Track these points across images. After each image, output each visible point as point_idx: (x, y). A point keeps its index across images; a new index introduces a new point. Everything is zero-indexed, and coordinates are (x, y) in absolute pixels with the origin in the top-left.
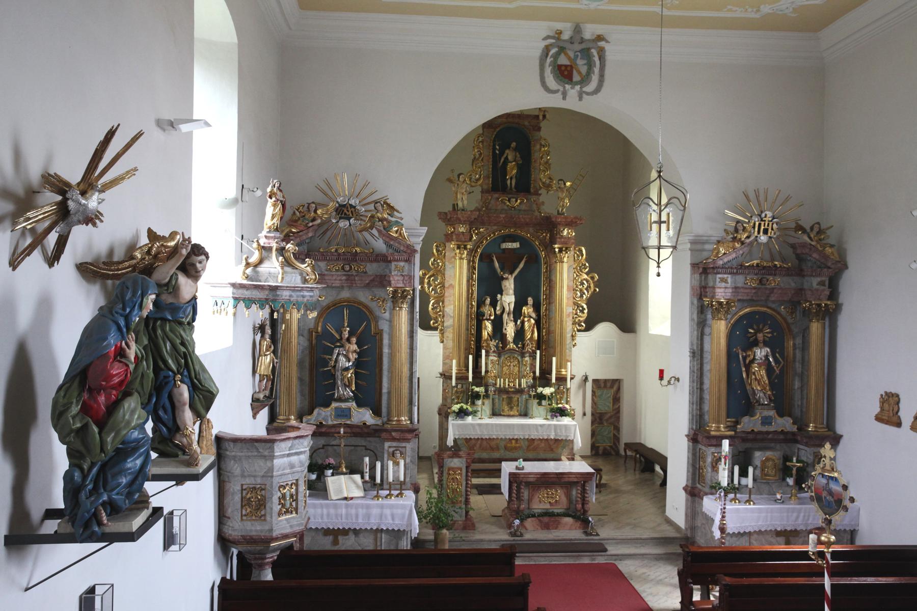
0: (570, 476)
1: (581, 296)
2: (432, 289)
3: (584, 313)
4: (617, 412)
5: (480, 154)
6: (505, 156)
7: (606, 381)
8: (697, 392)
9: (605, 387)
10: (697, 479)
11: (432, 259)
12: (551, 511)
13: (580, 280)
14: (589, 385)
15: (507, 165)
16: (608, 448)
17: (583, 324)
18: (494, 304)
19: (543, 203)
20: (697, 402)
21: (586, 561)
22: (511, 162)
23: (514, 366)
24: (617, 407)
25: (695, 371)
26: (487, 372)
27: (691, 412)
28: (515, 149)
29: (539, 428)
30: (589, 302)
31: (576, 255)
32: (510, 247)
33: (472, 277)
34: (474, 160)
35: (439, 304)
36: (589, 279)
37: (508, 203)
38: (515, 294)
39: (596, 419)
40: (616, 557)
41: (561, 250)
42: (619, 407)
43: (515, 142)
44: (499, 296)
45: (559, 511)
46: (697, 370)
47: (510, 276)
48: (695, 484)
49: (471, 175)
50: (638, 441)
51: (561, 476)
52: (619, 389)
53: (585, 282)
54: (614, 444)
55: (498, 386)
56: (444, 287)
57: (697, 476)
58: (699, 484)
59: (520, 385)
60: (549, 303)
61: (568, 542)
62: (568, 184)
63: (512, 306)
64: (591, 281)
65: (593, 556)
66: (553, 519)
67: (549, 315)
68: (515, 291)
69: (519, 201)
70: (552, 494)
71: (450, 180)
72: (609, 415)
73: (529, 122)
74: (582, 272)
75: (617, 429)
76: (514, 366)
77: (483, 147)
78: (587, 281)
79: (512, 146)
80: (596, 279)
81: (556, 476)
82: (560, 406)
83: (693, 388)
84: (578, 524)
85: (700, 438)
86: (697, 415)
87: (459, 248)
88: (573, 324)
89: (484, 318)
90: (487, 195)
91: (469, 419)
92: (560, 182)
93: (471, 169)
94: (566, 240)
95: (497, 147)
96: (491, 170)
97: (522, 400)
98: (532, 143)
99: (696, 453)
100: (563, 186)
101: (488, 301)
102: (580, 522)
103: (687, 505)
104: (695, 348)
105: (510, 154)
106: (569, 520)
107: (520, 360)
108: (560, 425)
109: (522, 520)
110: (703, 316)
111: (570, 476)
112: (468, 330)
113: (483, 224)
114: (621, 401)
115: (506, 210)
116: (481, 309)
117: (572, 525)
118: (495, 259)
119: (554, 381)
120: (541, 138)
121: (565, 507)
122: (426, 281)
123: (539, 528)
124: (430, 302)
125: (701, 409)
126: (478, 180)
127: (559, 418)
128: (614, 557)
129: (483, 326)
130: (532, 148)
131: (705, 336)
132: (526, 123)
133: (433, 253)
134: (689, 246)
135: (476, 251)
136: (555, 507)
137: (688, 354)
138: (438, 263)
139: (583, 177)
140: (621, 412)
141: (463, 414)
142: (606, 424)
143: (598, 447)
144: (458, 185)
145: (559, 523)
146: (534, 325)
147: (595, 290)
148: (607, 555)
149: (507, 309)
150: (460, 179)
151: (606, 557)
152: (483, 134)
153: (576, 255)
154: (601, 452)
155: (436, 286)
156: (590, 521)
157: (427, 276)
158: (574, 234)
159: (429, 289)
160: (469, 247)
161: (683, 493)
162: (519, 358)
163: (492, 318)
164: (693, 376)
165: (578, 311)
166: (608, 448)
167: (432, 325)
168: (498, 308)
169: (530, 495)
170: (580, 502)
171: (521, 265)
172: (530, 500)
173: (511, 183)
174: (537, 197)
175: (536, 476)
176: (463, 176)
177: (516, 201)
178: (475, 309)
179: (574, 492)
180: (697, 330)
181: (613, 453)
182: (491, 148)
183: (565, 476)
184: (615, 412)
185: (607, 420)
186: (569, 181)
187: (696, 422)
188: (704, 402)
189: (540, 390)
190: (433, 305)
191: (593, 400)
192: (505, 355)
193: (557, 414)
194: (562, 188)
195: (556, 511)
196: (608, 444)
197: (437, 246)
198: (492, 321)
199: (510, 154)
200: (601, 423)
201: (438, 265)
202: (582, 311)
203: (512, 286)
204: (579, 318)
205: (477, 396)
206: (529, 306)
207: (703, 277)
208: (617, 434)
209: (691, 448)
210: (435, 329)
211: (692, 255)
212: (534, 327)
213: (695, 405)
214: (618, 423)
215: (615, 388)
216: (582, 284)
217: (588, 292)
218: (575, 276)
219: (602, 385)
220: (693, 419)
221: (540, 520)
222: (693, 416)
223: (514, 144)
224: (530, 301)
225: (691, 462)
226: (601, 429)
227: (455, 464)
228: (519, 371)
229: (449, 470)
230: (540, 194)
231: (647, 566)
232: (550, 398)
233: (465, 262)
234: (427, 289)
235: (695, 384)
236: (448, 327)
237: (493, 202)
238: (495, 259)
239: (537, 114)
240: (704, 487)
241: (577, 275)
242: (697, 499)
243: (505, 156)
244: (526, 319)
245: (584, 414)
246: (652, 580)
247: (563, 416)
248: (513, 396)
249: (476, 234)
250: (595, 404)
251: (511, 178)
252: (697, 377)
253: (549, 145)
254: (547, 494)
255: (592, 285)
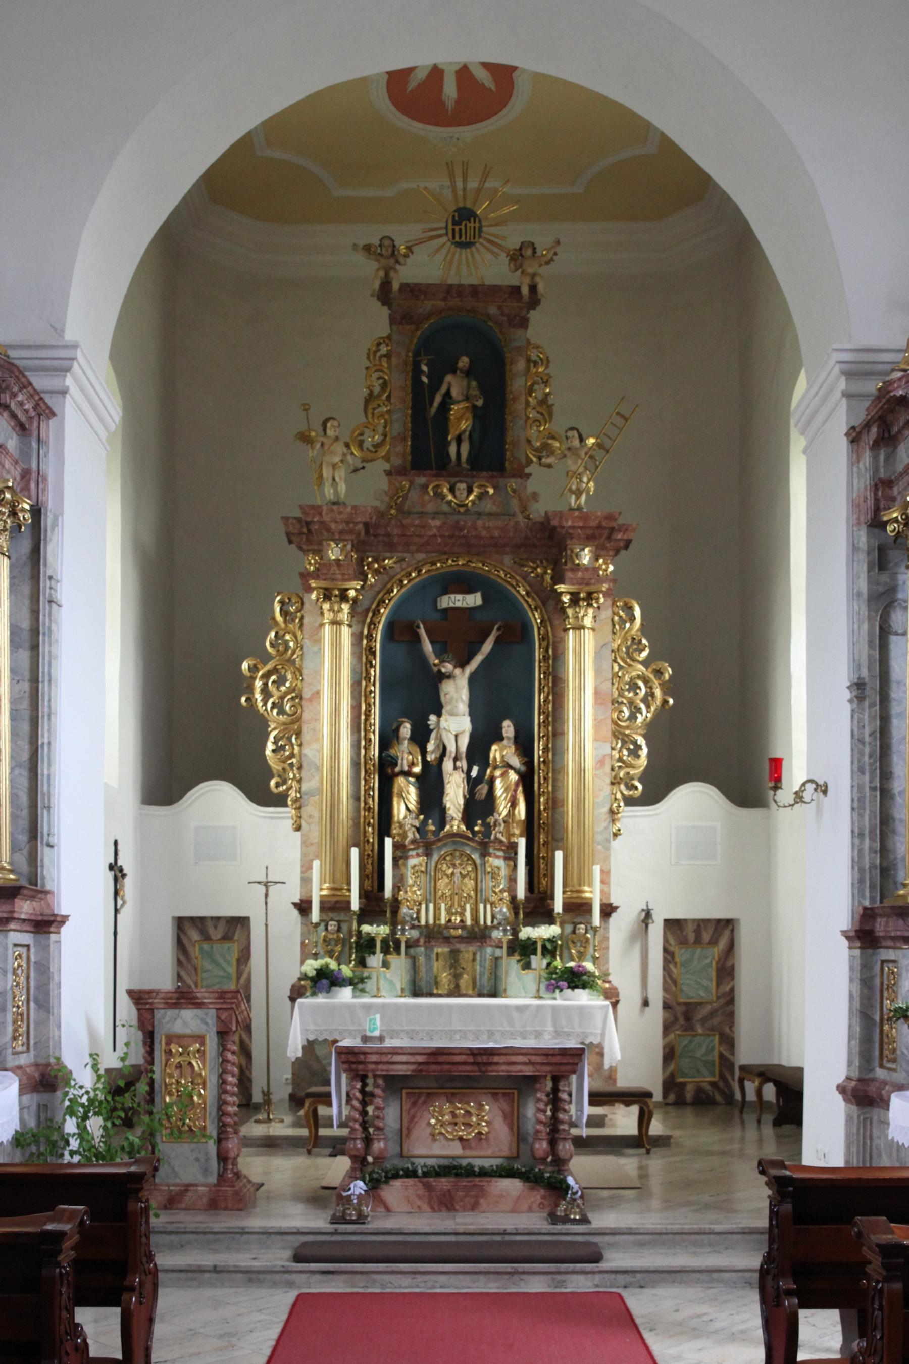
0: (514, 1059)
1: (633, 717)
2: (274, 705)
3: (638, 757)
4: (730, 1000)
5: (384, 385)
6: (443, 390)
7: (701, 924)
8: (872, 798)
9: (698, 941)
10: (877, 1053)
11: (273, 634)
12: (464, 1163)
13: (627, 679)
14: (656, 931)
15: (450, 409)
16: (708, 1088)
17: (637, 783)
18: (421, 737)
19: (535, 496)
20: (872, 831)
21: (536, 1285)
22: (458, 402)
23: (463, 876)
24: (727, 989)
25: (867, 739)
26: (397, 888)
27: (857, 863)
28: (468, 373)
29: (515, 1014)
30: (651, 731)
31: (616, 618)
32: (458, 604)
33: (368, 673)
34: (370, 398)
35: (289, 739)
36: (652, 676)
37: (450, 497)
38: (471, 714)
39: (676, 1019)
40: (628, 1278)
41: (575, 600)
42: (732, 990)
43: (467, 355)
44: (433, 718)
45: (486, 1163)
46: (872, 734)
47: (458, 671)
48: (872, 1070)
49: (361, 434)
50: (776, 1062)
51: (485, 1059)
52: (731, 947)
53: (641, 684)
54: (722, 1076)
55: (423, 922)
56: (301, 698)
57: (877, 1045)
58: (881, 1066)
59: (475, 919)
60: (555, 734)
61: (498, 1238)
62: (591, 441)
63: (464, 742)
64: (656, 683)
65: (559, 1273)
66: (464, 1182)
67: (553, 761)
68: (471, 706)
69: (476, 491)
70: (468, 1113)
71: (305, 438)
72: (708, 1008)
73: (500, 308)
74: (634, 660)
75: (729, 1041)
76: (463, 876)
77: (389, 368)
78: (646, 681)
79: (460, 365)
80: (667, 677)
81: (471, 1059)
82: (572, 964)
83: (861, 788)
84: (538, 1195)
85: (880, 926)
86: (872, 867)
87: (327, 597)
88: (612, 783)
89: (397, 769)
90: (400, 478)
91: (345, 994)
92: (570, 434)
93: (365, 420)
94: (587, 575)
95: (425, 368)
96: (409, 419)
97: (483, 960)
98: (508, 355)
99: (872, 977)
100: (576, 442)
101: (406, 730)
102: (542, 1192)
103: (848, 1135)
104: (865, 673)
105: (455, 385)
106: (512, 1186)
107: (478, 862)
108: (567, 1009)
109: (374, 1185)
110: (885, 578)
111: (514, 1059)
112: (358, 799)
113: (391, 546)
114: (736, 975)
115: (445, 514)
116: (392, 752)
117: (518, 1198)
118: (422, 631)
119: (558, 907)
120: (528, 341)
121: (506, 1153)
122: (258, 684)
123: (425, 1207)
124: (268, 734)
125: (884, 850)
126: (377, 446)
127: (568, 992)
128: (621, 1278)
129: (396, 790)
130: (507, 367)
131: (893, 638)
132: (493, 310)
133: (274, 619)
134: (842, 385)
135: (376, 612)
136: (475, 1153)
137: (847, 695)
138: (286, 643)
139: (626, 419)
140: (736, 1003)
141: (325, 981)
142: (700, 1031)
143: (683, 1085)
144: (322, 444)
145: (482, 1192)
146: (517, 784)
147: (665, 702)
148: (606, 1272)
149: (451, 748)
150: (328, 432)
151: (597, 1278)
152: (389, 337)
153: (616, 618)
154: (689, 1097)
155: (282, 698)
156: (568, 1187)
157: (260, 673)
158: (611, 568)
159: (265, 704)
160: (352, 593)
161: (839, 1098)
162: (476, 856)
163: (417, 770)
164: (861, 753)
165: (625, 752)
166: (708, 1088)
167: (275, 790)
168: (430, 747)
169: (405, 1120)
170: (543, 1135)
171: (487, 647)
172: (404, 1134)
173: (458, 454)
174: (519, 481)
175: (412, 1059)
176: (335, 423)
177: (470, 491)
178: (375, 751)
179: (530, 1111)
180: (870, 619)
181: (718, 1098)
182: (410, 368)
183: (496, 1059)
184: (722, 1001)
185: (704, 1021)
186: (593, 436)
187: (872, 887)
188: (894, 831)
189: (526, 932)
190: (275, 743)
191: (666, 968)
192: (440, 848)
193: (561, 983)
194: (576, 449)
195: (478, 1163)
196: (707, 1078)
197: (282, 602)
198: (418, 777)
199: (455, 385)
200: (689, 1026)
201: (287, 648)
202: (635, 752)
203: (465, 694)
204: (628, 770)
205: (366, 946)
206: (505, 742)
207: (882, 458)
208: (726, 1053)
209: (857, 963)
210: (280, 801)
211: (849, 409)
212: (515, 791)
213: (867, 841)
214: (731, 1028)
215: (723, 943)
216: (634, 687)
217: (648, 707)
218: (616, 668)
219: (691, 937)
220: (861, 881)
221: (429, 1188)
222: (861, 870)
223: (464, 362)
224: (508, 729)
225: (857, 1004)
226: (690, 1042)
227: (185, 1024)
228: (476, 890)
229: (168, 1043)
230: (528, 476)
231: (715, 1300)
232: (550, 949)
233: (346, 632)
234: (260, 704)
235: (867, 778)
236: (311, 794)
237: (414, 495)
238: (422, 631)
239: (516, 283)
240: (895, 1070)
241: (621, 667)
242: (876, 1112)
243: (443, 390)
244: (498, 773)
245: (646, 1003)
246: (716, 1331)
247: (576, 987)
248: (462, 947)
249: (376, 572)
250: (675, 982)
251: (459, 440)
252: (870, 757)
253: (548, 361)
254: (453, 1115)
255: (658, 692)
